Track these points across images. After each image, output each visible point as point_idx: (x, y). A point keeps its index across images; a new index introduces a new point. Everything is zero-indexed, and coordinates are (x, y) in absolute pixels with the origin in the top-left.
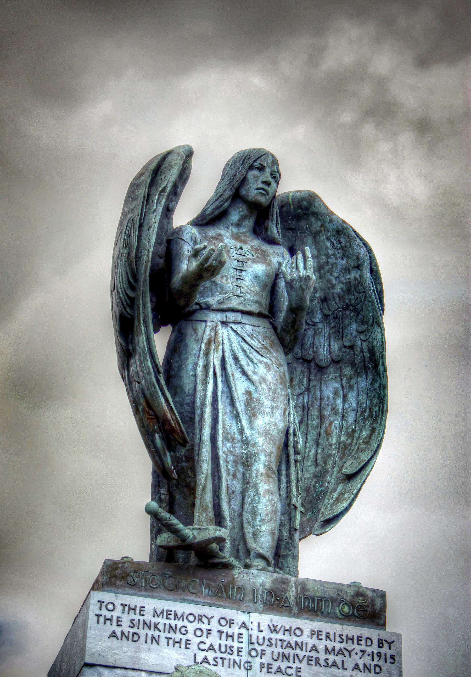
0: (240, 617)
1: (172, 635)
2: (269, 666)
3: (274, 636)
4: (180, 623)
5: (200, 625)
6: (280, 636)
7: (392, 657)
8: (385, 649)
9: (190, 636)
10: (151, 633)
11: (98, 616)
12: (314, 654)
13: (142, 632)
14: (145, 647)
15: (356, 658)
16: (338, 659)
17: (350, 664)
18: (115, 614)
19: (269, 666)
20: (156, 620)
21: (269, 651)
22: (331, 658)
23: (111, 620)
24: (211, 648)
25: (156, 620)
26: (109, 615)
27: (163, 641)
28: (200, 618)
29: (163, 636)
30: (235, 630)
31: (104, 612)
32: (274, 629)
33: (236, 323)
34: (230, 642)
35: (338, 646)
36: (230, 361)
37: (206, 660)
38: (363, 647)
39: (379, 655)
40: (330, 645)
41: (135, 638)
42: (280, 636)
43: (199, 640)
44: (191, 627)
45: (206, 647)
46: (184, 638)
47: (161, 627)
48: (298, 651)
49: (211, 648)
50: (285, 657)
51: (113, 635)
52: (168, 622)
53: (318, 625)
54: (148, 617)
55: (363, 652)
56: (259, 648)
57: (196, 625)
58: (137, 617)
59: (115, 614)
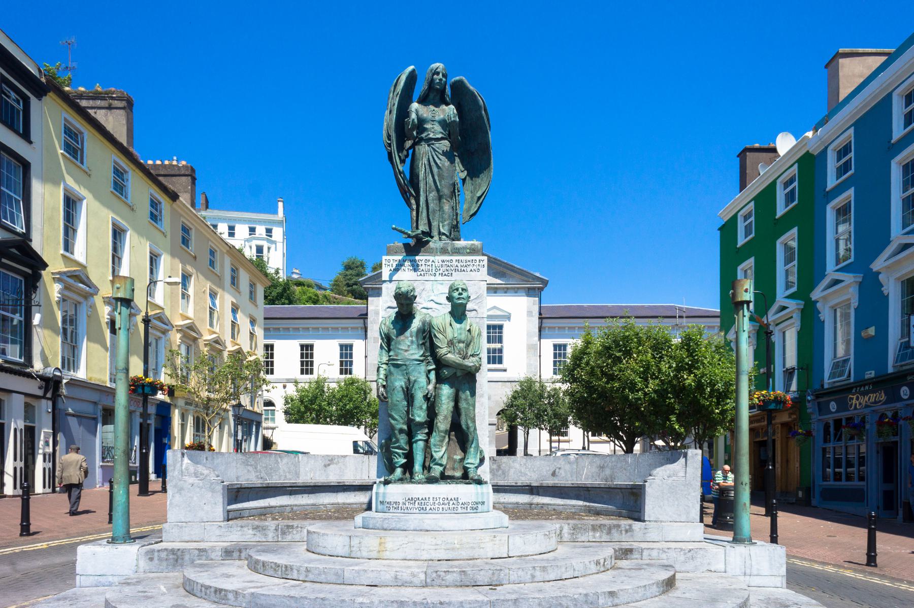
0: (431, 258)
15: (471, 268)
17: (469, 269)
30: (430, 263)
32: (443, 261)
36: (431, 160)
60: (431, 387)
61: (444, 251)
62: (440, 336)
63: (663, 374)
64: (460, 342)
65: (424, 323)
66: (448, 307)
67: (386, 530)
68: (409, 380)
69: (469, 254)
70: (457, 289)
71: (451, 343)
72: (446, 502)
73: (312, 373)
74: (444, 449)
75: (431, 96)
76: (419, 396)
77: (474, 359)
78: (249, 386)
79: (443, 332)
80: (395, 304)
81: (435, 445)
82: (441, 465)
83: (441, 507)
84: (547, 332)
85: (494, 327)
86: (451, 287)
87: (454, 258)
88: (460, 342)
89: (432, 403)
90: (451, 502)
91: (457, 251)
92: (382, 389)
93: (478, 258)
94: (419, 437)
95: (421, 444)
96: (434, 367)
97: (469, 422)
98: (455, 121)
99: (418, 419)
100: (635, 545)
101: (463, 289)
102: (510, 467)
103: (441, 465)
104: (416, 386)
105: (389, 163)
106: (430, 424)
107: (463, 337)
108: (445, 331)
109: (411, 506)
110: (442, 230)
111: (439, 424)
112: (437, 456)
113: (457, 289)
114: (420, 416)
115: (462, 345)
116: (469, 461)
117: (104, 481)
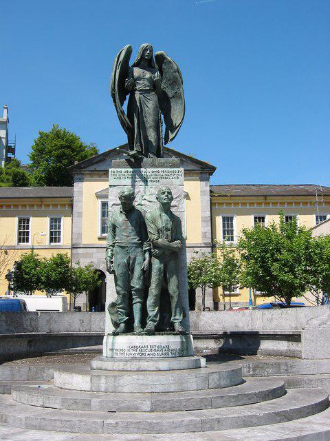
32: (153, 172)
53: (118, 169)
60: (146, 262)
61: (153, 165)
66: (158, 205)
67: (142, 371)
69: (171, 167)
70: (164, 193)
73: (28, 241)
75: (142, 63)
77: (209, 302)
79: (154, 222)
80: (119, 202)
83: (156, 353)
84: (217, 207)
86: (159, 191)
87: (160, 170)
89: (147, 274)
91: (162, 166)
93: (177, 170)
100: (175, 363)
105: (113, 104)
106: (144, 293)
109: (134, 352)
114: (136, 283)
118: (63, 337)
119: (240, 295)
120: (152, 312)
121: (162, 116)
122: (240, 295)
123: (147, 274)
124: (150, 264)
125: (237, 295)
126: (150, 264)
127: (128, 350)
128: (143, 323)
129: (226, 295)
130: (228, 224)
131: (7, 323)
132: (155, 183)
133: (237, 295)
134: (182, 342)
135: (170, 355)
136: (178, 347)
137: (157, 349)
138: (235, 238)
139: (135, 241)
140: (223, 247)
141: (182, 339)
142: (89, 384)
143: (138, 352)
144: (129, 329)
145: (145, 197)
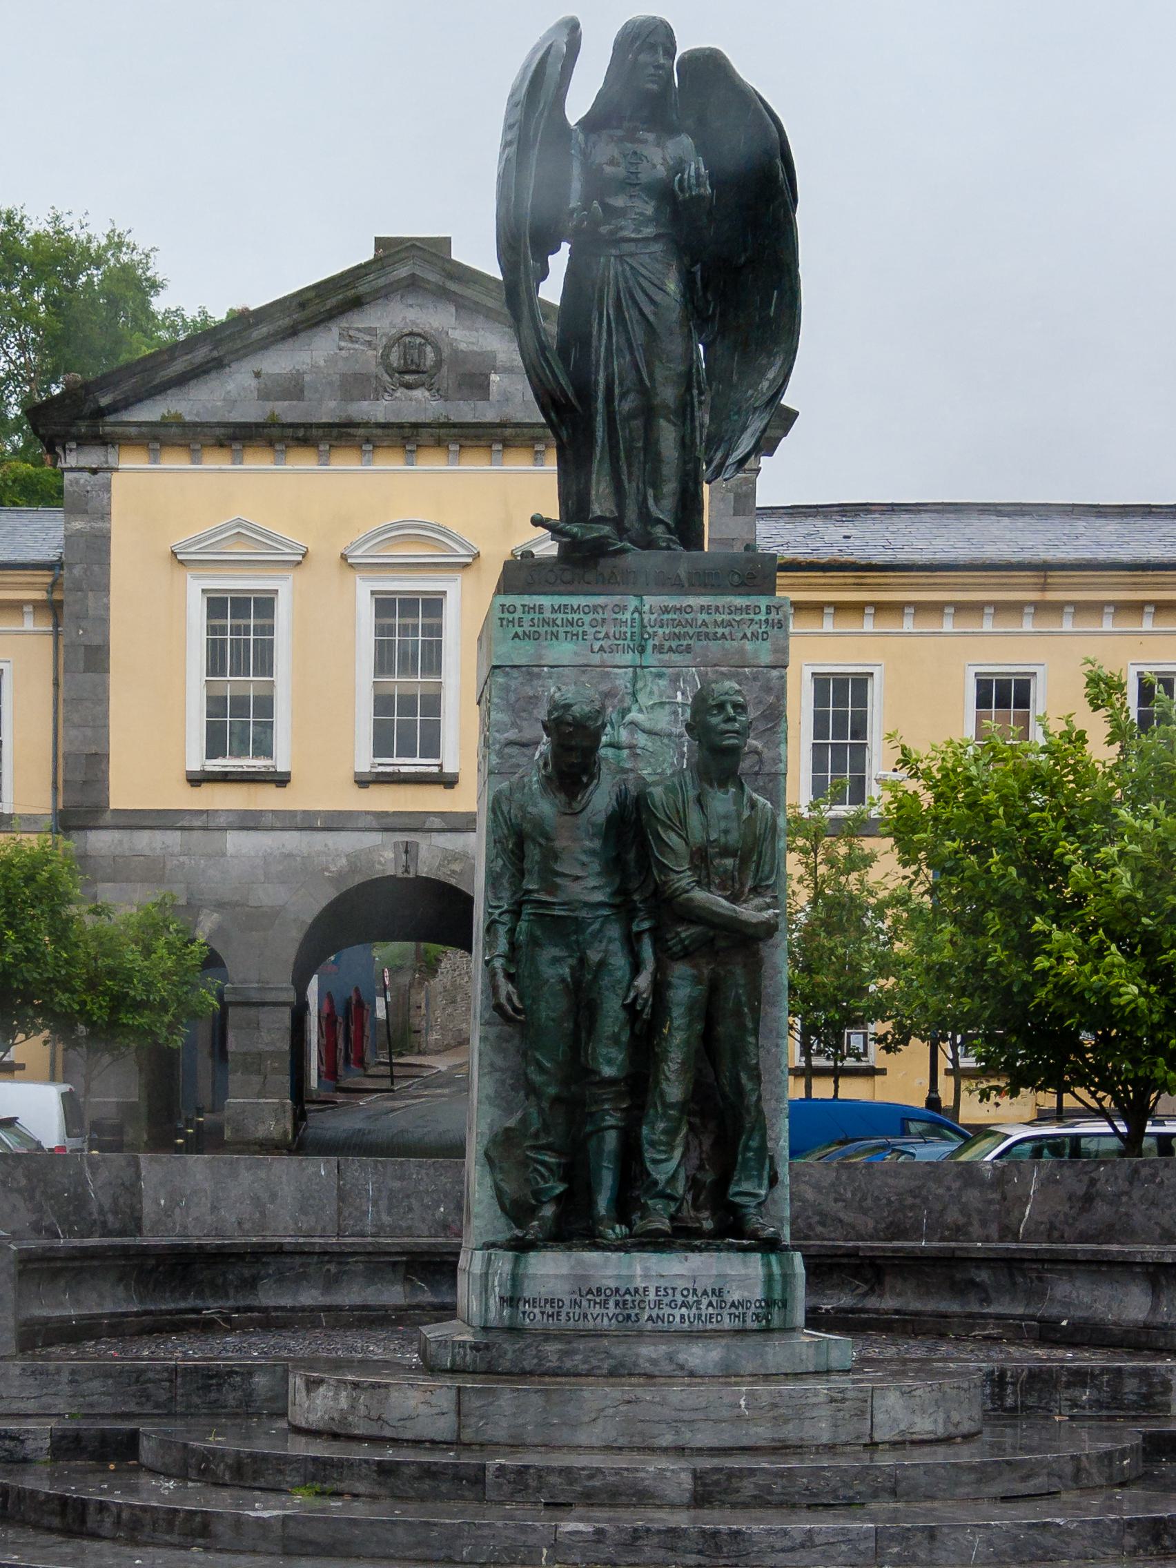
1: (569, 629)
2: (662, 646)
3: (665, 617)
4: (576, 616)
5: (596, 616)
6: (670, 616)
7: (779, 621)
8: (774, 616)
9: (586, 628)
10: (549, 629)
11: (501, 619)
12: (704, 629)
13: (542, 630)
14: (545, 643)
16: (727, 631)
18: (516, 616)
19: (662, 646)
20: (554, 616)
21: (660, 631)
22: (720, 631)
23: (513, 621)
24: (607, 636)
25: (554, 616)
26: (510, 617)
27: (561, 635)
28: (595, 609)
29: (561, 630)
31: (506, 615)
32: (666, 610)
33: (631, 255)
34: (624, 629)
35: (726, 617)
37: (601, 649)
38: (752, 616)
39: (767, 621)
40: (719, 618)
41: (536, 637)
42: (670, 616)
43: (593, 630)
44: (587, 619)
45: (601, 636)
46: (581, 630)
47: (559, 622)
48: (688, 629)
49: (607, 636)
50: (677, 637)
51: (516, 636)
52: (565, 616)
54: (547, 614)
55: (752, 620)
56: (650, 630)
57: (591, 616)
58: (537, 616)
59: (516, 616)
60: (643, 981)
62: (672, 839)
63: (838, 1178)
64: (726, 852)
65: (622, 798)
68: (582, 961)
70: (721, 707)
71: (701, 859)
72: (691, 1299)
74: (678, 1153)
76: (612, 1007)
78: (63, 997)
79: (681, 826)
81: (653, 1144)
82: (671, 1198)
83: (677, 1313)
85: (409, 604)
88: (726, 852)
89: (645, 1030)
90: (705, 1302)
92: (505, 987)
94: (610, 1121)
95: (611, 1140)
96: (646, 925)
97: (744, 1078)
98: (700, 198)
99: (608, 1071)
101: (736, 706)
102: (637, 1355)
103: (671, 1198)
104: (606, 981)
107: (733, 838)
108: (684, 823)
110: (656, 512)
111: (664, 1085)
112: (661, 1174)
113: (721, 707)
114: (610, 1063)
115: (729, 862)
116: (746, 1186)
117: (801, 1055)
118: (937, 1259)
119: (882, 1072)
120: (668, 1165)
121: (701, 347)
122: (882, 1072)
123: (645, 1030)
124: (660, 987)
125: (871, 1072)
126: (660, 987)
127: (575, 1303)
128: (624, 1208)
129: (822, 1072)
130: (840, 718)
131: (32, 1198)
132: (675, 658)
133: (871, 1072)
134: (769, 1278)
135: (727, 1323)
136: (758, 1293)
137: (679, 1299)
138: (873, 790)
139: (599, 897)
140: (816, 833)
141: (768, 1265)
142: (452, 1418)
143: (612, 1309)
144: (573, 1229)
145: (634, 715)
